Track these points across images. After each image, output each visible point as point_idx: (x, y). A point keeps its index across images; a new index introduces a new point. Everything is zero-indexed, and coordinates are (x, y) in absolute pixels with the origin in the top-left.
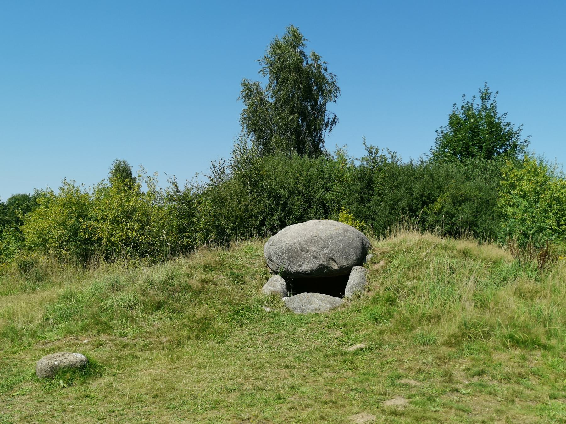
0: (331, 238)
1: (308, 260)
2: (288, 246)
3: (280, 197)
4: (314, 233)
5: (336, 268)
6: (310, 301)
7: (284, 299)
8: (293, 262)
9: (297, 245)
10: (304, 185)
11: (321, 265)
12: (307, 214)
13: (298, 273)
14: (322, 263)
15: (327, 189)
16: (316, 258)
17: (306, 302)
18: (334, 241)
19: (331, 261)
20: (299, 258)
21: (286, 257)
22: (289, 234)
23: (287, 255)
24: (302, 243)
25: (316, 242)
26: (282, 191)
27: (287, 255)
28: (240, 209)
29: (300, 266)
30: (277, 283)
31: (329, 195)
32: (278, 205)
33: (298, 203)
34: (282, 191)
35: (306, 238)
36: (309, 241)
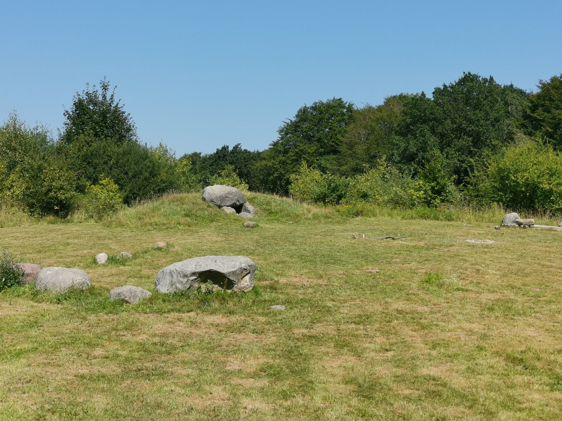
36: (227, 193)
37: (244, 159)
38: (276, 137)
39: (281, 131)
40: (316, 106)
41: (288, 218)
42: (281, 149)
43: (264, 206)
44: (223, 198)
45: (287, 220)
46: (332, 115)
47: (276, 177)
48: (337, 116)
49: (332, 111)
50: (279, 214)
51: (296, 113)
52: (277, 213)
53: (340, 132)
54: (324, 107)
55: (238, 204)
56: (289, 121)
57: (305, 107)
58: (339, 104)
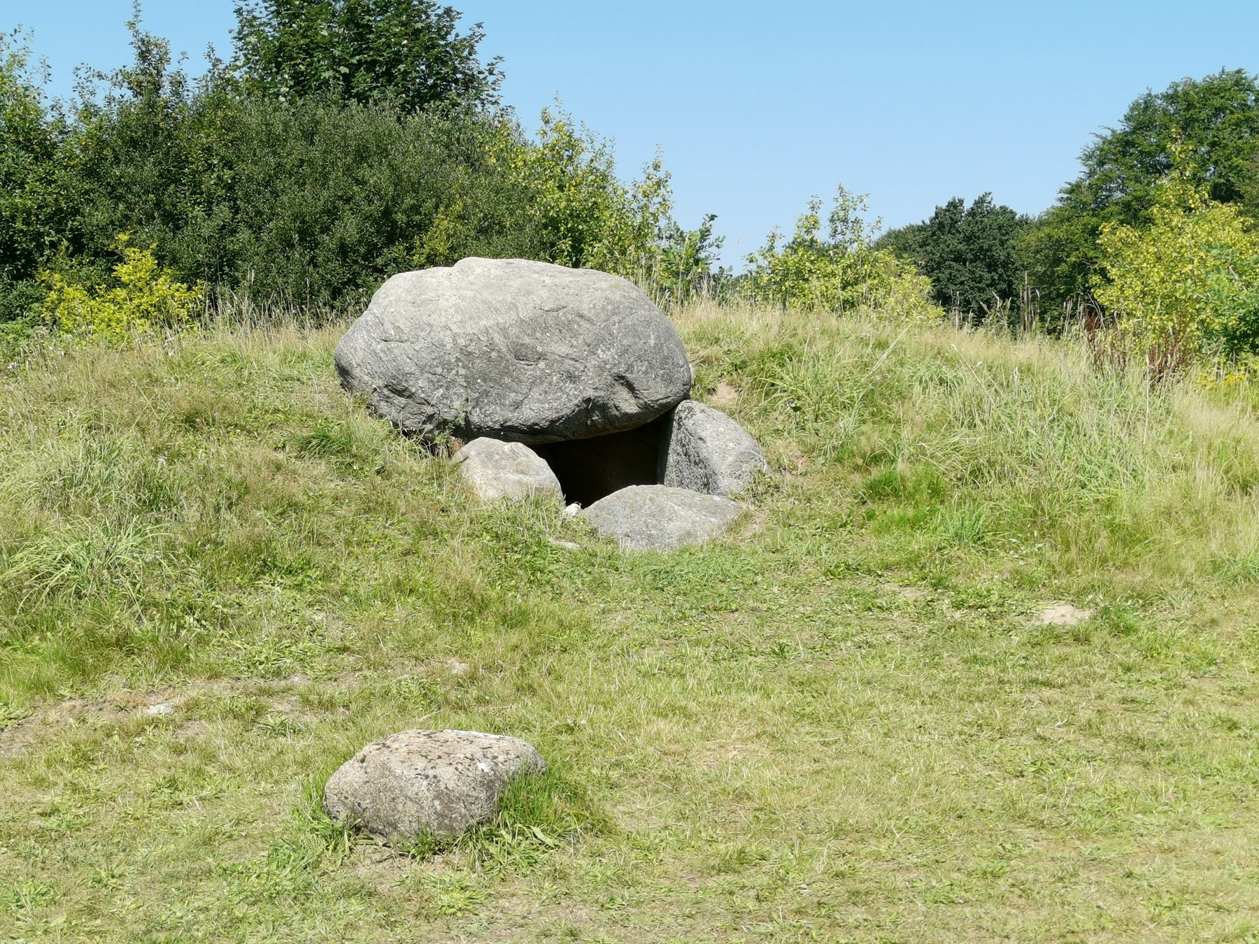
2: (462, 342)
8: (486, 393)
9: (497, 338)
11: (588, 400)
14: (590, 393)
16: (572, 377)
18: (628, 322)
20: (507, 380)
21: (461, 381)
25: (565, 329)
27: (462, 372)
29: (517, 406)
30: (507, 475)
36: (537, 324)
37: (1000, 228)
38: (1076, 172)
39: (1089, 157)
40: (1176, 91)
41: (1032, 557)
42: (1087, 197)
43: (847, 422)
44: (495, 363)
45: (1022, 581)
46: (1219, 110)
47: (1074, 265)
48: (1232, 113)
49: (1217, 102)
50: (950, 518)
51: (1126, 111)
52: (936, 492)
53: (1239, 151)
54: (1197, 93)
55: (629, 405)
56: (1108, 134)
57: (1149, 95)
58: (1237, 83)
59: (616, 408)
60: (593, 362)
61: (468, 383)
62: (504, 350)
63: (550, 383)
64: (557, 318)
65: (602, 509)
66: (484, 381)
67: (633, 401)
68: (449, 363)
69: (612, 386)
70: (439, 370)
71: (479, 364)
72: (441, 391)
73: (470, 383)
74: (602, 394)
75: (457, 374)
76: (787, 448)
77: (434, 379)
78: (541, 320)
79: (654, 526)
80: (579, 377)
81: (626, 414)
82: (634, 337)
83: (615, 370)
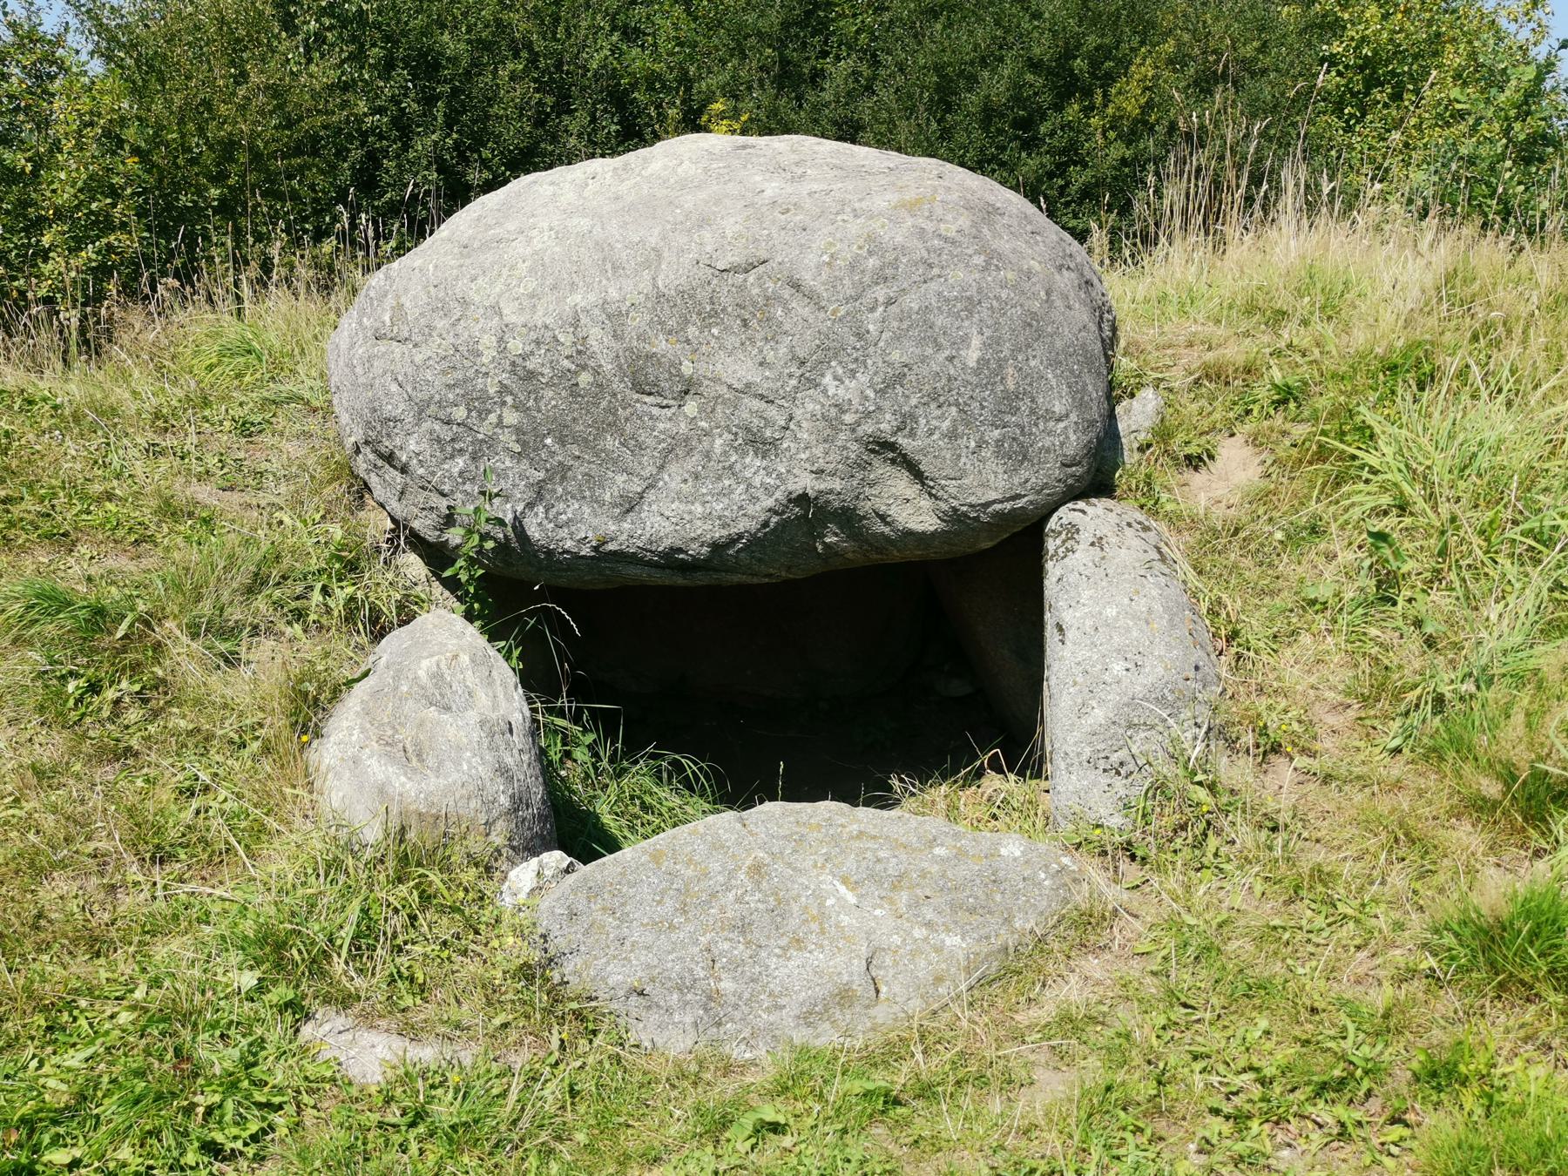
0: (881, 278)
1: (693, 462)
2: (516, 346)
3: (436, 66)
4: (729, 236)
5: (916, 514)
6: (778, 912)
7: (523, 875)
8: (563, 471)
9: (598, 338)
10: (536, 14)
11: (803, 500)
12: (554, 139)
13: (605, 558)
14: (805, 482)
15: (631, 34)
16: (759, 444)
17: (743, 927)
18: (912, 302)
19: (881, 469)
20: (611, 442)
21: (508, 439)
22: (519, 248)
23: (511, 418)
24: (637, 322)
25: (755, 317)
26: (446, 37)
27: (511, 418)
28: (242, 108)
29: (630, 505)
30: (443, 712)
31: (638, 60)
32: (429, 100)
33: (511, 89)
34: (446, 37)
35: (671, 276)
36: (695, 308)
59: (883, 518)
60: (810, 405)
61: (524, 444)
62: (608, 367)
63: (707, 455)
64: (741, 288)
65: (593, 893)
66: (562, 441)
67: (926, 503)
68: (484, 397)
69: (864, 466)
70: (460, 413)
71: (552, 399)
72: (460, 462)
73: (528, 448)
74: (837, 485)
75: (500, 424)
76: (1309, 675)
77: (446, 433)
78: (702, 295)
79: (736, 965)
80: (774, 443)
81: (909, 533)
82: (921, 342)
83: (868, 428)
